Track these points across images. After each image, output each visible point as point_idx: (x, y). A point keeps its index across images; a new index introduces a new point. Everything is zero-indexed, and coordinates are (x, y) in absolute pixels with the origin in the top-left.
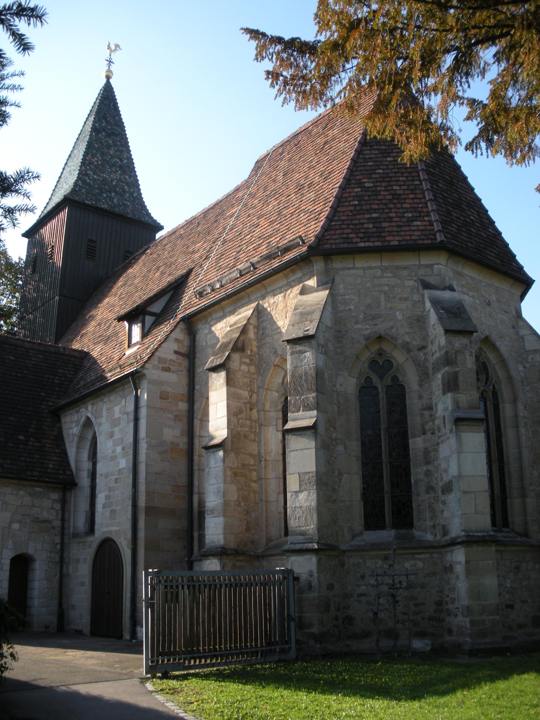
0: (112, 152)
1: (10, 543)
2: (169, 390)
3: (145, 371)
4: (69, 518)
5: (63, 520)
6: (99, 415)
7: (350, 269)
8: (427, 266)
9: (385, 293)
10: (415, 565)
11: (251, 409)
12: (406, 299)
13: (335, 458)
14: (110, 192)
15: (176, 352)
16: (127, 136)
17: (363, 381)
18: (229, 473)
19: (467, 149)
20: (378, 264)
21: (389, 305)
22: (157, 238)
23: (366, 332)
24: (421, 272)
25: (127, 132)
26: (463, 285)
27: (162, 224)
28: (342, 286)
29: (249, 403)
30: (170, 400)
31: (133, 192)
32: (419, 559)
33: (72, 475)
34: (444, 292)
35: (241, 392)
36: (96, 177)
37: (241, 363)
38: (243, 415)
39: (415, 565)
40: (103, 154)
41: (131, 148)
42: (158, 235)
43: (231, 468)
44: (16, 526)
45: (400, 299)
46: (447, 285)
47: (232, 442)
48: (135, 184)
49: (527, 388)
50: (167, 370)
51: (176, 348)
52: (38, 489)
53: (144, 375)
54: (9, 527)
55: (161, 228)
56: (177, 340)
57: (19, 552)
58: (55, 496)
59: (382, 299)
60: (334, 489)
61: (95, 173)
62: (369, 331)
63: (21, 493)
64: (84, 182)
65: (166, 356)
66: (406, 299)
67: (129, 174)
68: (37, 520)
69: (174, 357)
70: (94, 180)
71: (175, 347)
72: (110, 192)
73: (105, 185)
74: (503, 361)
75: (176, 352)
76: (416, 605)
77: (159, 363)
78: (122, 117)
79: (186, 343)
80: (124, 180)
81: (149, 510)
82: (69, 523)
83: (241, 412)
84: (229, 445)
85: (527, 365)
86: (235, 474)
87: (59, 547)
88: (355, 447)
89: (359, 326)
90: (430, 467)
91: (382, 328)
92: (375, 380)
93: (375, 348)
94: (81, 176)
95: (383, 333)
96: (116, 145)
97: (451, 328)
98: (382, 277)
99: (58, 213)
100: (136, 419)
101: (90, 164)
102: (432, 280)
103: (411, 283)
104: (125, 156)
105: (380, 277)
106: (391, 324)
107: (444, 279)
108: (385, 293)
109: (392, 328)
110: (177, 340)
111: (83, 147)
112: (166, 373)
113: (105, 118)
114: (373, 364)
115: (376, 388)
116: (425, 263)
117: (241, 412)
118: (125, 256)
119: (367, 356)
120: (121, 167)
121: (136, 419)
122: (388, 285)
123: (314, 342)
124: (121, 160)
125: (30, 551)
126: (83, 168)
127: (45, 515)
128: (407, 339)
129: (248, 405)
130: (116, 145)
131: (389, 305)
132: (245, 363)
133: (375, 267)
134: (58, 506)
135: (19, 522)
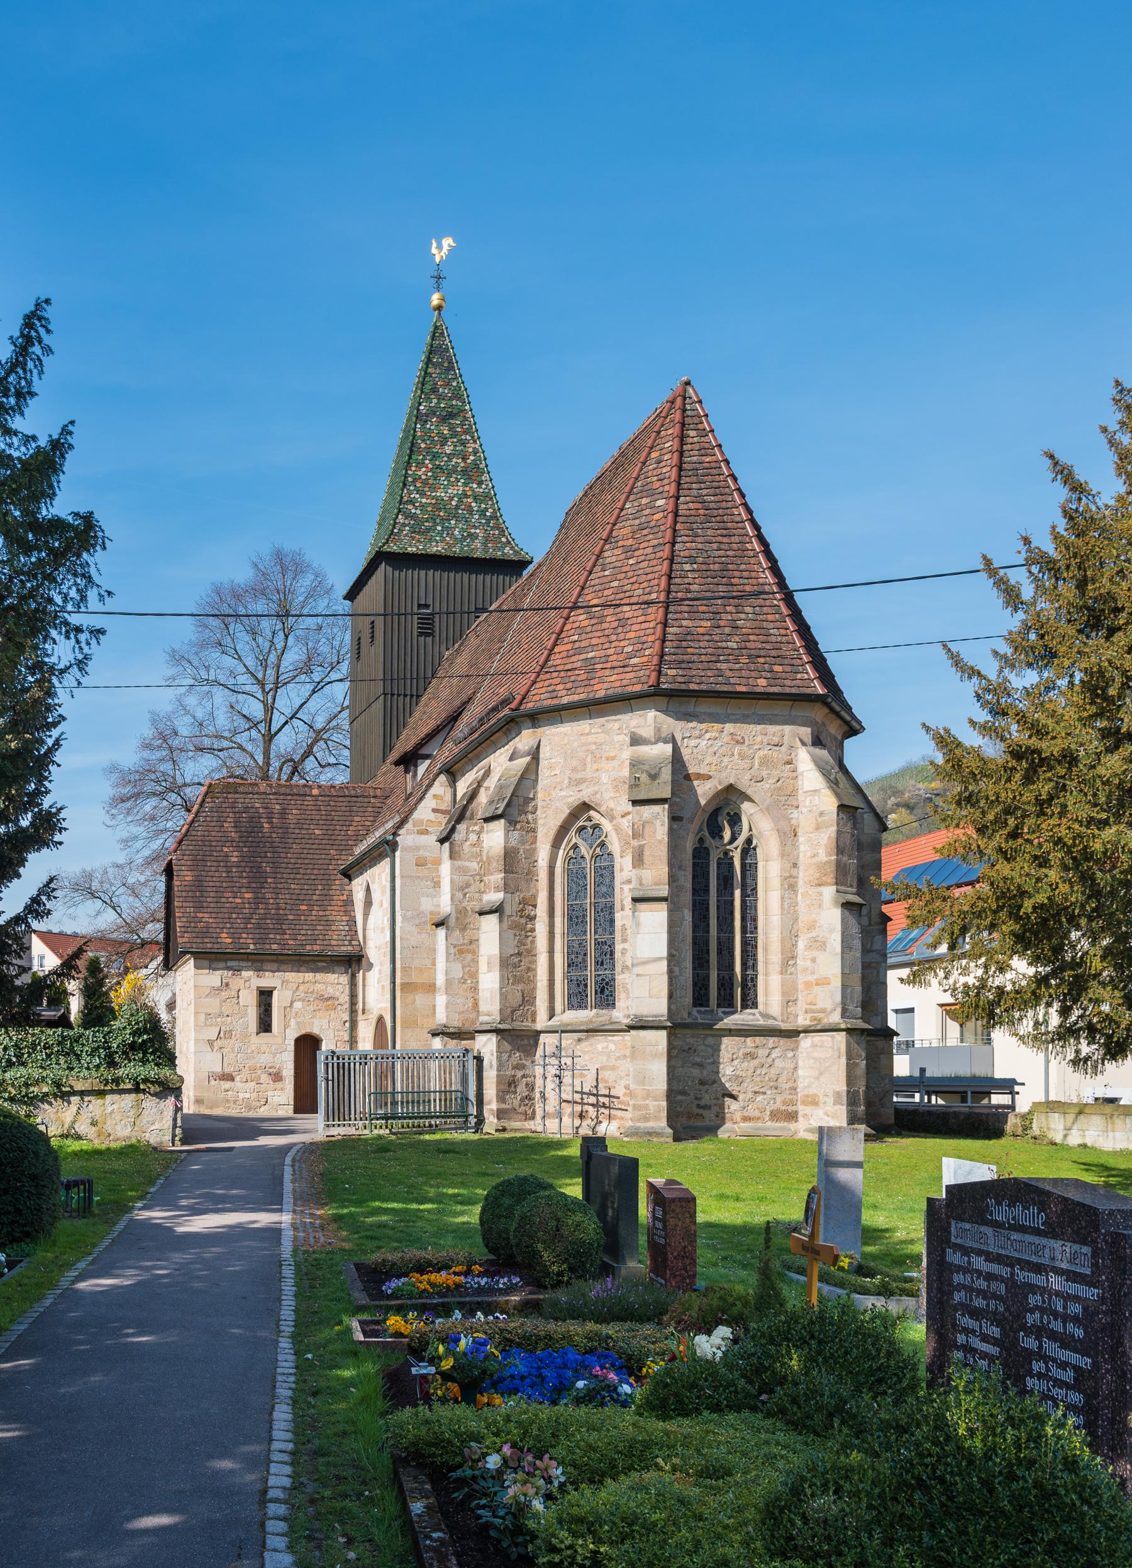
0: (448, 449)
10: (607, 1047)
12: (613, 758)
15: (435, 811)
19: (397, 763)
21: (595, 767)
23: (570, 800)
30: (429, 866)
32: (612, 1041)
34: (654, 747)
36: (424, 500)
38: (472, 889)
39: (607, 1047)
40: (435, 456)
47: (457, 919)
51: (434, 806)
54: (291, 1006)
57: (303, 1032)
61: (423, 494)
66: (613, 758)
69: (432, 816)
70: (422, 505)
73: (440, 510)
75: (435, 811)
76: (698, 1106)
84: (452, 921)
86: (461, 952)
87: (347, 1024)
89: (563, 793)
90: (626, 946)
99: (376, 569)
101: (415, 480)
104: (470, 450)
106: (596, 788)
112: (423, 837)
124: (464, 459)
125: (316, 1031)
127: (330, 991)
128: (612, 805)
130: (454, 434)
131: (595, 767)
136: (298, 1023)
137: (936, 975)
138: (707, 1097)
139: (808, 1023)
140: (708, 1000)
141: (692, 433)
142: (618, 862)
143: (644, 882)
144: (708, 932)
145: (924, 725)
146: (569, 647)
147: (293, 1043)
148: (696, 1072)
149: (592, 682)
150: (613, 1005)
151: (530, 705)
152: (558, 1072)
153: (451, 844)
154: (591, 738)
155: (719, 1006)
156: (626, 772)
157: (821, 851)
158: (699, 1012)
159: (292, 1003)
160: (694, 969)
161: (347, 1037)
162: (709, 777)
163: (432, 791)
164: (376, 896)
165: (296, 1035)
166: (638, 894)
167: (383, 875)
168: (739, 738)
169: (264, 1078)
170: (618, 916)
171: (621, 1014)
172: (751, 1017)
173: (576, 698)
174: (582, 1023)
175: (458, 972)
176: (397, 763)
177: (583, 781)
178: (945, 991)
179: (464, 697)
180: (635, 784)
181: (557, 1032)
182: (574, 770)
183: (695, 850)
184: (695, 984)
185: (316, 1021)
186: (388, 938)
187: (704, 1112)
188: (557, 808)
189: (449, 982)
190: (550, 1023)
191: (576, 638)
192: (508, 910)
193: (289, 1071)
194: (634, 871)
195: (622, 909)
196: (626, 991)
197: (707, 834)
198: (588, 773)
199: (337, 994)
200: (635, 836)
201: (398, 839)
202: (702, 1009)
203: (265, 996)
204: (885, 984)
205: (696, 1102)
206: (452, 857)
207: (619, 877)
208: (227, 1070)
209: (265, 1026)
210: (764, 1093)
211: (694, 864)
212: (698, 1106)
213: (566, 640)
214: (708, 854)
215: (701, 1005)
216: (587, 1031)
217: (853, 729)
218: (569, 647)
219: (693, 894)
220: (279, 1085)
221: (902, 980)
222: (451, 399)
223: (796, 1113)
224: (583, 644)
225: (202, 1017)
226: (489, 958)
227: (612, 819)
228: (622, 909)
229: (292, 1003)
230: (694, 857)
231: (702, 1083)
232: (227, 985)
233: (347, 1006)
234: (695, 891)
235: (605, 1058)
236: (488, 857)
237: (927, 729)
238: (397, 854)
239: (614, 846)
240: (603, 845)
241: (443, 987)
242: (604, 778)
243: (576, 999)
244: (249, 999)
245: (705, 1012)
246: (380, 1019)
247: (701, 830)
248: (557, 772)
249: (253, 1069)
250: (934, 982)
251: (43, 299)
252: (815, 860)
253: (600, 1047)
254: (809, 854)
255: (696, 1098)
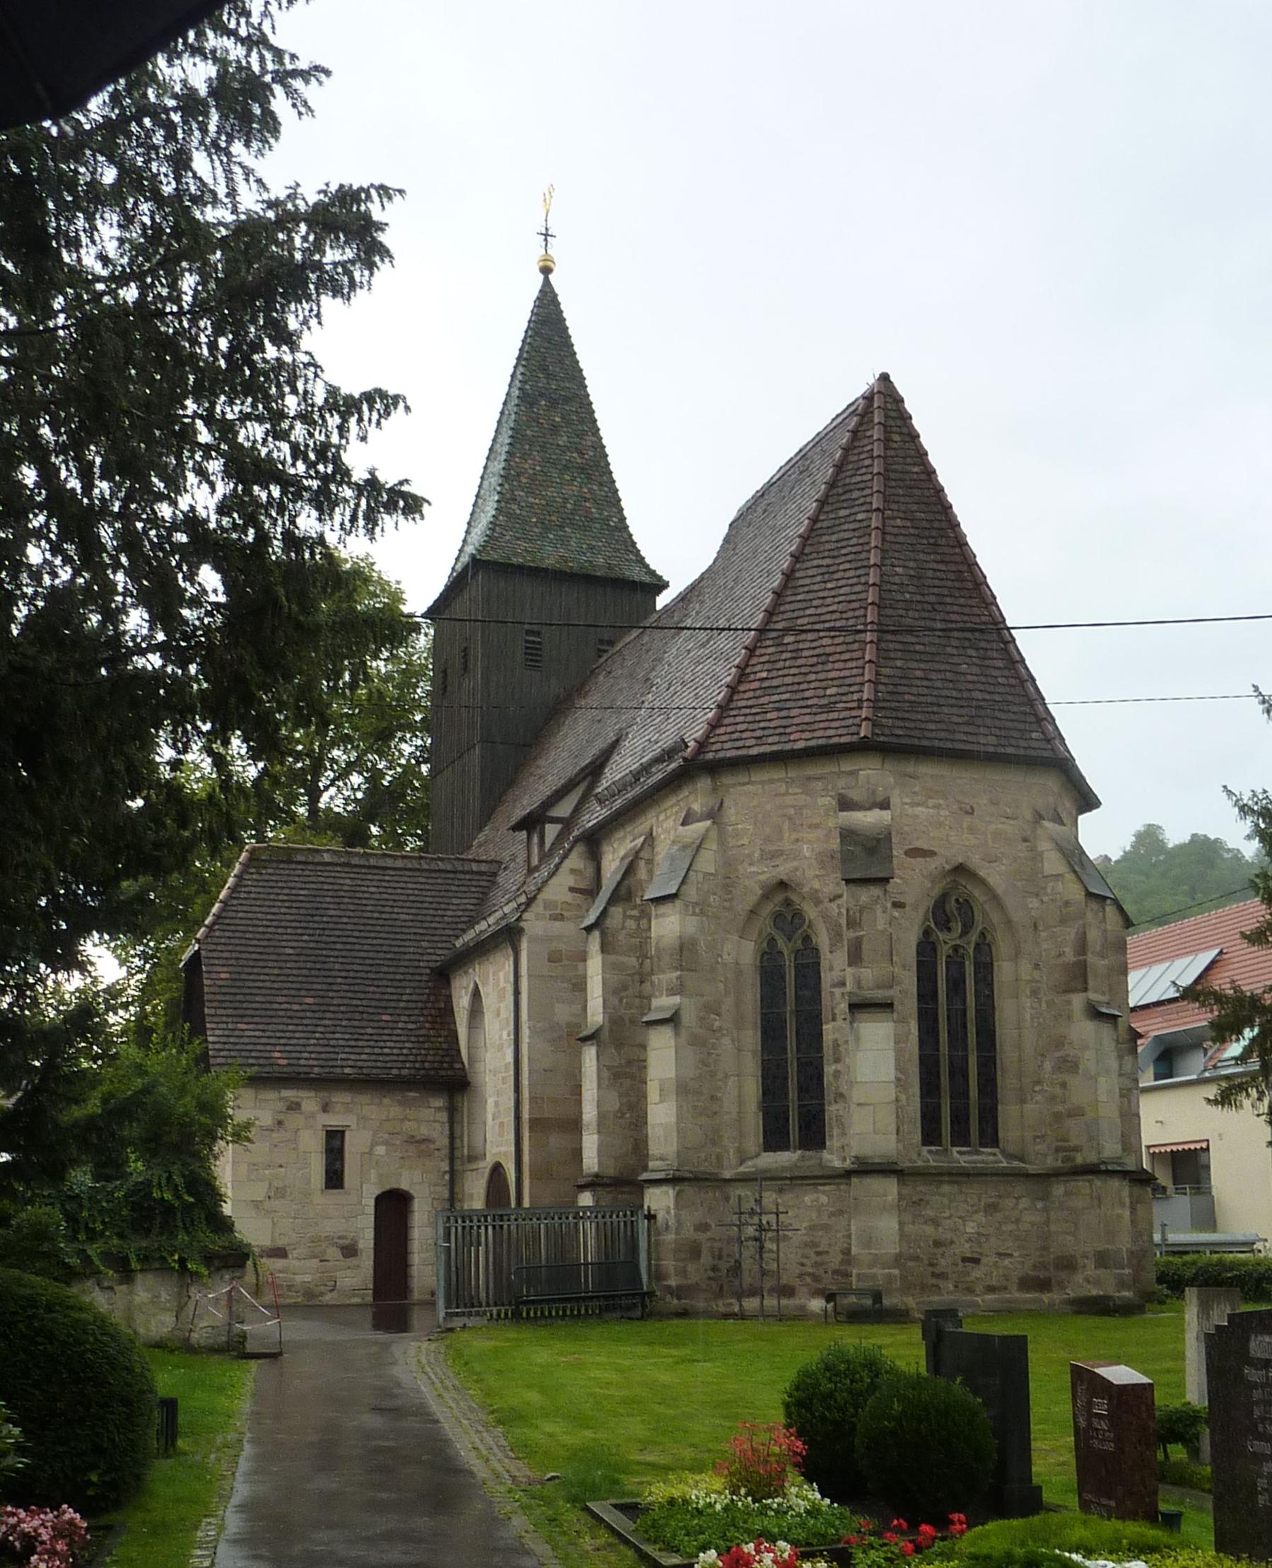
1: (373, 1175)
2: (562, 946)
3: (522, 924)
4: (462, 1135)
5: (452, 1137)
6: (485, 983)
7: (745, 784)
8: (852, 773)
9: (790, 818)
11: (642, 982)
12: (817, 826)
13: (718, 1055)
14: (561, 527)
15: (572, 890)
16: (591, 398)
17: (765, 944)
18: (606, 1074)
20: (782, 774)
21: (794, 836)
22: (659, 607)
23: (762, 877)
24: (841, 783)
25: (589, 390)
26: (915, 793)
27: (666, 578)
28: (732, 811)
29: (640, 974)
31: (609, 518)
32: (824, 1192)
33: (463, 1069)
34: (868, 813)
35: (625, 959)
37: (626, 917)
38: (630, 992)
40: (543, 448)
41: (599, 424)
42: (662, 600)
43: (609, 1068)
44: (381, 1150)
45: (810, 827)
46: (879, 799)
47: (611, 1031)
48: (613, 500)
49: (1043, 934)
50: (559, 917)
51: (572, 884)
52: (412, 1094)
53: (521, 930)
54: (370, 1153)
55: (661, 585)
56: (573, 871)
57: (388, 1187)
58: (439, 1102)
59: (786, 826)
60: (713, 1098)
61: (531, 493)
62: (767, 876)
63: (386, 1101)
64: (510, 515)
65: (556, 898)
66: (817, 826)
67: (599, 479)
68: (412, 1140)
69: (569, 897)
70: (531, 506)
71: (571, 881)
72: (561, 527)
74: (994, 897)
75: (572, 890)
77: (545, 908)
78: (578, 357)
79: (590, 872)
80: (588, 496)
81: (534, 1123)
82: (462, 1141)
83: (625, 988)
84: (605, 1035)
85: (1045, 899)
87: (447, 1177)
88: (752, 1037)
89: (753, 869)
90: (839, 1067)
91: (783, 870)
92: (781, 943)
93: (779, 898)
94: (503, 504)
95: (785, 878)
96: (568, 423)
97: (855, 876)
98: (787, 794)
100: (517, 993)
102: (855, 795)
103: (826, 800)
105: (784, 795)
106: (796, 864)
107: (874, 792)
108: (790, 818)
109: (797, 869)
110: (573, 871)
111: (505, 439)
112: (557, 924)
113: (544, 369)
114: (777, 917)
115: (780, 953)
116: (848, 769)
117: (625, 988)
118: (599, 650)
119: (769, 908)
120: (582, 469)
121: (517, 993)
122: (794, 806)
123: (678, 903)
124: (581, 454)
125: (404, 1186)
126: (506, 486)
127: (424, 1131)
128: (816, 885)
129: (637, 978)
132: (631, 917)
133: (779, 780)
134: (444, 1117)
135: (386, 1143)
136: (380, 1175)
137: (1248, 1095)
138: (943, 1262)
139: (1059, 1164)
140: (940, 1135)
141: (896, 438)
142: (826, 957)
143: (863, 982)
144: (938, 1050)
145: (1225, 787)
146: (756, 685)
147: (372, 1203)
148: (929, 1229)
149: (788, 730)
150: (821, 1145)
151: (710, 756)
152: (757, 1234)
153: (603, 935)
154: (789, 800)
155: (953, 1145)
156: (835, 844)
157: (1067, 950)
158: (929, 1152)
159: (371, 1149)
160: (922, 1097)
161: (446, 1195)
162: (932, 853)
163: (568, 864)
164: (488, 1001)
165: (378, 1192)
166: (855, 1000)
167: (501, 974)
168: (968, 808)
169: (334, 1253)
170: (827, 1028)
171: (833, 1159)
172: (991, 1158)
173: (767, 749)
174: (784, 1169)
175: (614, 1103)
176: (517, 827)
177: (780, 853)
178: (1258, 1115)
179: (600, 744)
180: (846, 858)
181: (756, 1180)
182: (768, 840)
183: (919, 945)
184: (923, 1117)
185: (405, 1173)
186: (510, 1058)
187: (941, 1283)
188: (745, 887)
189: (602, 1116)
190: (742, 1169)
191: (764, 675)
192: (688, 1018)
193: (367, 1241)
194: (849, 970)
195: (834, 1020)
196: (841, 1125)
197: (933, 926)
198: (786, 845)
199: (435, 1135)
200: (851, 924)
201: (522, 924)
202: (933, 1148)
203: (334, 1142)
204: (1138, 1116)
205: (931, 1269)
206: (604, 949)
207: (827, 978)
208: (280, 1243)
209: (334, 1179)
210: (1011, 1255)
211: (918, 962)
212: (934, 1275)
213: (752, 677)
214: (935, 950)
215: (932, 1144)
216: (791, 1179)
217: (1088, 801)
218: (756, 685)
219: (919, 1001)
220: (353, 1261)
221: (1209, 1100)
222: (562, 379)
223: (1050, 1279)
224: (775, 683)
225: (243, 1169)
226: (662, 1083)
227: (818, 902)
228: (834, 1020)
229: (371, 1149)
230: (918, 953)
231: (937, 1244)
232: (280, 1123)
233: (446, 1152)
234: (921, 997)
235: (814, 1216)
236: (658, 949)
237: (1230, 793)
238: (524, 945)
239: (822, 939)
240: (807, 939)
241: (594, 1124)
242: (806, 850)
243: (774, 1139)
244: (313, 1144)
245: (937, 1152)
246: (497, 1169)
247: (926, 919)
248: (746, 841)
249: (315, 1240)
250: (1247, 1103)
251: (266, 152)
252: (1060, 961)
253: (807, 1199)
254: (1053, 953)
255: (931, 1265)
